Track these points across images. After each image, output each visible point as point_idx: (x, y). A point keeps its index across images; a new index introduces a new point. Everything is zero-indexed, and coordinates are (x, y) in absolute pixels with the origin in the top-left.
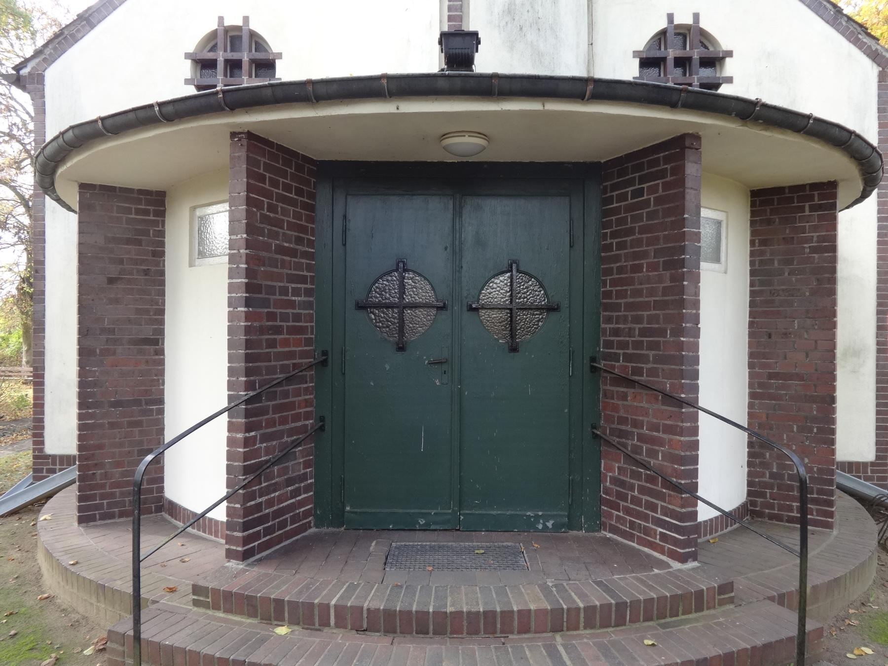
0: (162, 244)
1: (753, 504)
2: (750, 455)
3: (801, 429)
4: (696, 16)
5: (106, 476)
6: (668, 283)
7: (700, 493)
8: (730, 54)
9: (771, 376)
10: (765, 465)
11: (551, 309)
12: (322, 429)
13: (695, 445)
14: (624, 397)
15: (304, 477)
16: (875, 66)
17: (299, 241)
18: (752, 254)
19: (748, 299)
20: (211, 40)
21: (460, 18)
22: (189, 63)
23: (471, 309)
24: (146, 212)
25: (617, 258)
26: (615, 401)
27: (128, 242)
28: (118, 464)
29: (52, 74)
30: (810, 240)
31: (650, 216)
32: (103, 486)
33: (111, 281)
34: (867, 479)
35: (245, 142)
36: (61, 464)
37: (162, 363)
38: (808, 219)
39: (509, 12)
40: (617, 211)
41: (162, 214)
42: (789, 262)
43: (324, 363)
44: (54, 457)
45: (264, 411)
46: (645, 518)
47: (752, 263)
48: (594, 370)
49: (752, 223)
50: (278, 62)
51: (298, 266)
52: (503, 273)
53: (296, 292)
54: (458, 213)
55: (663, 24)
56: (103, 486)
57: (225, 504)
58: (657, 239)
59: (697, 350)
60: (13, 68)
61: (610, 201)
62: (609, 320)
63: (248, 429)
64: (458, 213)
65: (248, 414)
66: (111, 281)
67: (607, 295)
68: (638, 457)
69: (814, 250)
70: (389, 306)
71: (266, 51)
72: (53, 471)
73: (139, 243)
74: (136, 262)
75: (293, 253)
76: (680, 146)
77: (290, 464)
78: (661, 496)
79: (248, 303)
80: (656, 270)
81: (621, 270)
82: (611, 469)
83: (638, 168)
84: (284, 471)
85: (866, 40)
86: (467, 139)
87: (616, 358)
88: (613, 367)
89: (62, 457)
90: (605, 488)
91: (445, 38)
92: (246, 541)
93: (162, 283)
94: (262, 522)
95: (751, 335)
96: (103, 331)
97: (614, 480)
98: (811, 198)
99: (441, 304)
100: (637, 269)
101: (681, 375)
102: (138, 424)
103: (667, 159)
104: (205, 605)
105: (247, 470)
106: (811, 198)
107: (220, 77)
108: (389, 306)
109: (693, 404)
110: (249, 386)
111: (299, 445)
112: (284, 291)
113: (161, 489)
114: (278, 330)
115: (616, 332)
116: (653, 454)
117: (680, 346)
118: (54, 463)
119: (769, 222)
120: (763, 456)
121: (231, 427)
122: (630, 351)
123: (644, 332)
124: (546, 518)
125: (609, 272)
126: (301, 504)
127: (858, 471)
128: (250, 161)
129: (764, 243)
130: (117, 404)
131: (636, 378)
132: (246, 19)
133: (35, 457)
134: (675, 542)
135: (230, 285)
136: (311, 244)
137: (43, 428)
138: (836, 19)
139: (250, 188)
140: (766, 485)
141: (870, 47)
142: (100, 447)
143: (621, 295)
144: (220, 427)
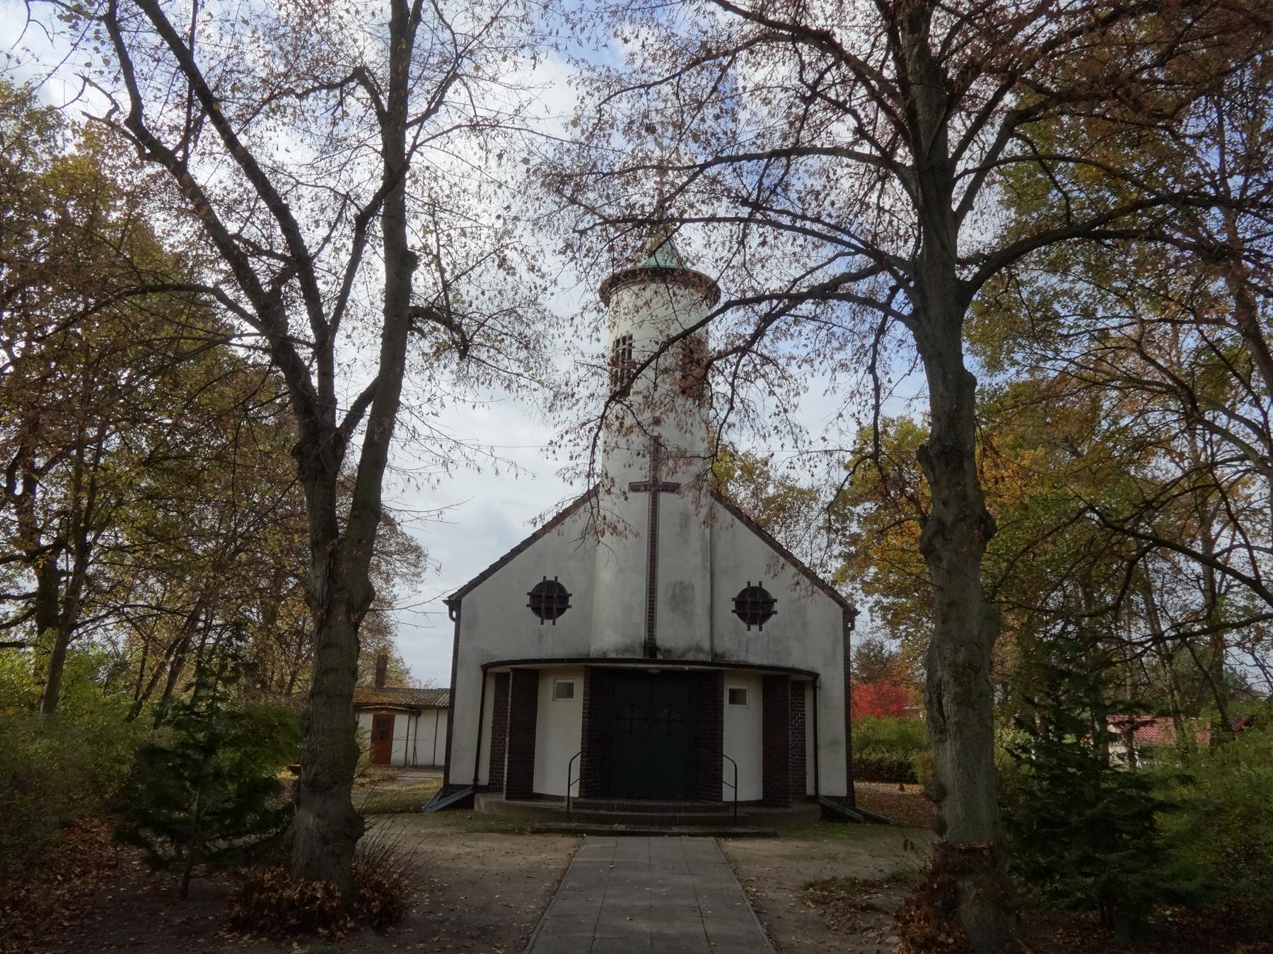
55: (746, 586)
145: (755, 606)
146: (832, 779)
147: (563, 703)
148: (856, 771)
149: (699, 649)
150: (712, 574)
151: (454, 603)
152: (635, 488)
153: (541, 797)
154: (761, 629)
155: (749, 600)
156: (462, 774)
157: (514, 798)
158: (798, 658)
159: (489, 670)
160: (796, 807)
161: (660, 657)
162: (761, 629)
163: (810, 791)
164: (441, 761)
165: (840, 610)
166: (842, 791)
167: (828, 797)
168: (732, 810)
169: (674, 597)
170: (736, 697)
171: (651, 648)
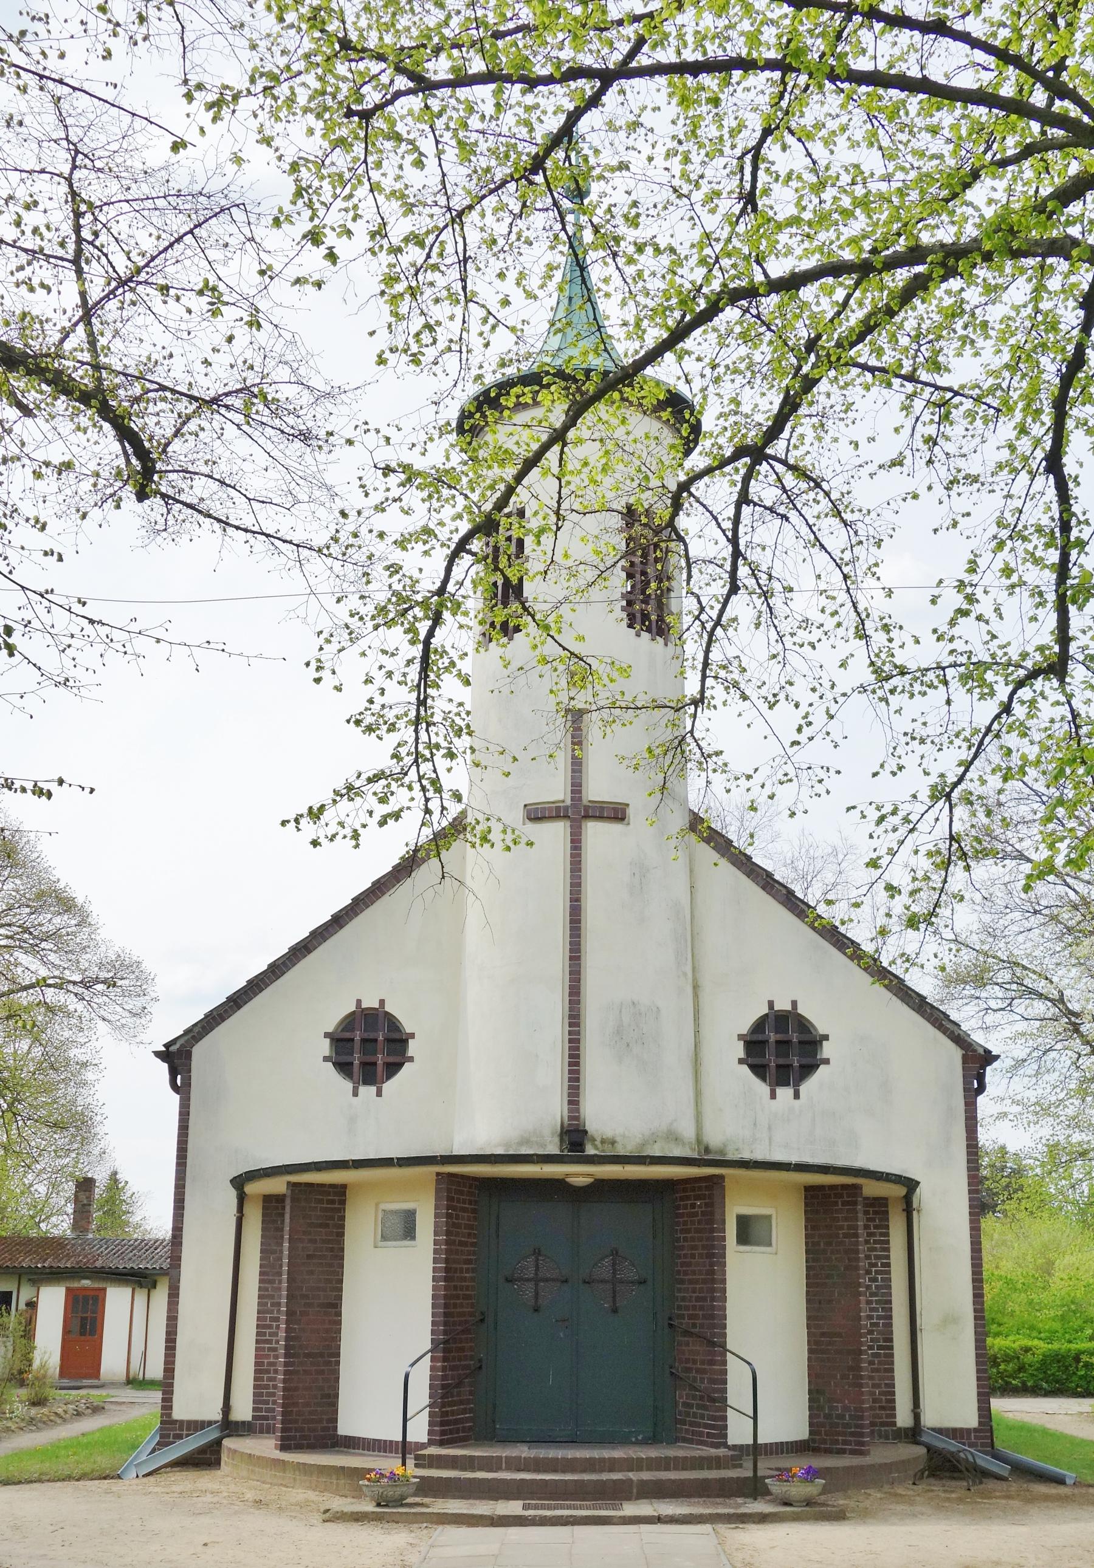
0: (343, 1226)
2: (810, 1400)
3: (843, 1377)
4: (794, 1003)
7: (729, 1402)
8: (826, 1037)
9: (823, 1334)
11: (642, 1282)
13: (725, 1372)
14: (688, 1345)
15: (468, 1402)
22: (328, 1040)
24: (333, 1202)
25: (682, 1248)
27: (321, 1226)
30: (841, 1228)
31: (699, 1222)
32: (296, 1421)
36: (188, 1429)
37: (340, 1323)
40: (682, 1215)
41: (343, 1202)
42: (829, 1244)
43: (482, 1321)
44: (182, 1422)
46: (699, 1425)
48: (671, 1326)
55: (765, 1010)
56: (296, 1421)
61: (678, 1207)
66: (309, 1257)
67: (679, 1272)
69: (846, 1236)
70: (528, 1280)
72: (180, 1437)
73: (327, 1226)
75: (465, 1244)
76: (716, 1182)
81: (685, 1256)
82: (681, 1397)
87: (682, 1317)
89: (189, 1422)
92: (443, 1433)
93: (342, 1258)
94: (449, 1424)
95: (808, 1301)
97: (685, 1404)
98: (841, 1196)
100: (693, 1256)
101: (714, 1326)
102: (322, 1372)
106: (841, 1196)
108: (528, 1280)
109: (723, 1345)
116: (702, 1380)
117: (713, 1308)
121: (433, 1359)
126: (467, 1420)
128: (449, 1190)
129: (813, 1228)
130: (308, 1355)
140: (823, 1425)
142: (296, 1389)
143: (686, 1273)
144: (427, 1361)
145: (783, 1049)
146: (946, 1392)
147: (397, 1253)
148: (998, 1376)
149: (674, 1137)
150: (696, 987)
151: (177, 1057)
152: (537, 814)
153: (352, 1444)
154: (797, 1096)
155: (773, 1037)
156: (198, 1399)
157: (299, 1447)
158: (871, 1148)
159: (251, 1188)
160: (881, 1454)
161: (590, 1150)
162: (797, 1096)
163: (903, 1418)
164: (155, 1370)
165: (956, 1053)
166: (969, 1419)
167: (940, 1431)
168: (748, 1464)
169: (619, 1031)
170: (750, 1231)
171: (574, 1138)
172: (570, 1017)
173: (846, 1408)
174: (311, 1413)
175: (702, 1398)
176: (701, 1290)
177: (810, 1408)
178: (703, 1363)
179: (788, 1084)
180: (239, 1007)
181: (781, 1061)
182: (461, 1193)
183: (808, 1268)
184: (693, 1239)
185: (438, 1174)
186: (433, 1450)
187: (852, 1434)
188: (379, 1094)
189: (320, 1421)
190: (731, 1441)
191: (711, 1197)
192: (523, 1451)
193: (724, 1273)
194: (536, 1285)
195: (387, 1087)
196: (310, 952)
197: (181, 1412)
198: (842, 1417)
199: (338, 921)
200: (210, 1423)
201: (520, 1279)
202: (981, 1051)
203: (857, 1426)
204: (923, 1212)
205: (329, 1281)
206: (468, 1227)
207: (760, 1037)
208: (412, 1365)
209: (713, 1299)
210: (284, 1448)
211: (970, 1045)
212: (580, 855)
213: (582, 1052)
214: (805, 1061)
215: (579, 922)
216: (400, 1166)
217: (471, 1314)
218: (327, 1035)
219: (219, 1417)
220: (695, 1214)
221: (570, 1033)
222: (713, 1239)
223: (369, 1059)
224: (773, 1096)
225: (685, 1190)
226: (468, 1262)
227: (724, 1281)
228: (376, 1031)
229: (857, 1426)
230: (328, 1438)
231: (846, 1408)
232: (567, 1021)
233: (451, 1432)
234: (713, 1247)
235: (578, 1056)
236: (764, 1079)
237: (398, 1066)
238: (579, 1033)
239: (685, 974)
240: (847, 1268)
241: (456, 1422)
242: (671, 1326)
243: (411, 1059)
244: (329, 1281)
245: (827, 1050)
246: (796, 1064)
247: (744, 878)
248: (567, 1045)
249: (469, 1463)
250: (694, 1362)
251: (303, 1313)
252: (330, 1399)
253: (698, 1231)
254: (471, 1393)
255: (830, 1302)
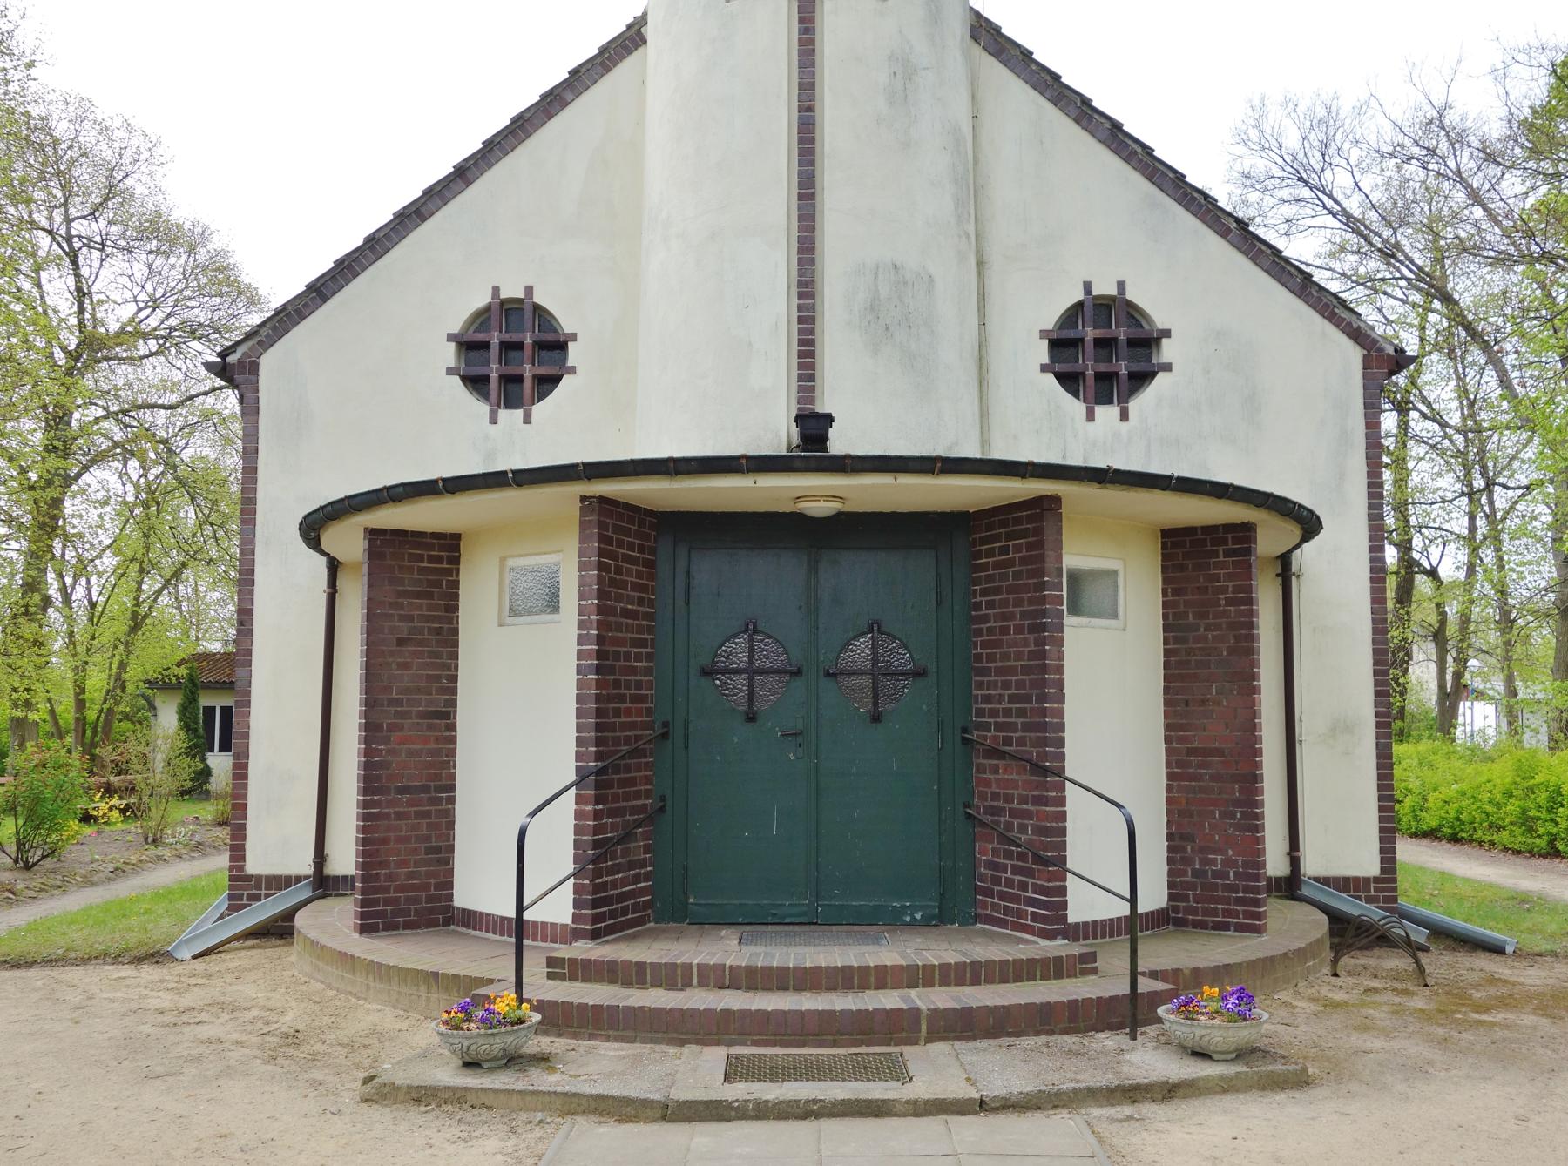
0: (456, 597)
1: (1176, 909)
2: (1170, 849)
3: (1224, 815)
4: (1121, 285)
5: (390, 877)
6: (1032, 648)
7: (1069, 866)
8: (1167, 333)
9: (1191, 752)
10: (1186, 861)
11: (919, 673)
12: (662, 809)
14: (995, 770)
15: (643, 864)
16: (1358, 348)
17: (641, 601)
18: (1165, 605)
19: (1162, 660)
20: (482, 318)
21: (813, 401)
22: (453, 345)
23: (827, 674)
24: (439, 560)
25: (986, 619)
26: (987, 776)
27: (419, 595)
28: (403, 864)
29: (269, 363)
30: (1224, 590)
31: (1017, 575)
32: (387, 890)
33: (401, 642)
34: (1369, 900)
35: (596, 506)
37: (453, 740)
38: (1223, 566)
39: (872, 309)
40: (985, 567)
42: (1202, 616)
43: (665, 736)
44: (259, 878)
45: (609, 785)
46: (1016, 899)
47: (1165, 617)
48: (966, 741)
49: (1164, 569)
50: (570, 344)
51: (640, 629)
52: (863, 634)
53: (638, 658)
54: (813, 569)
55: (1079, 296)
56: (387, 890)
57: (572, 880)
58: (1022, 600)
59: (1062, 717)
60: (219, 355)
61: (978, 555)
62: (980, 686)
63: (598, 800)
64: (813, 569)
65: (598, 785)
66: (401, 642)
67: (978, 658)
68: (1009, 834)
69: (1230, 602)
70: (737, 672)
71: (555, 331)
72: (257, 898)
73: (430, 595)
74: (428, 619)
76: (1046, 507)
77: (632, 845)
78: (1029, 873)
79: (599, 670)
80: (1021, 632)
81: (991, 631)
83: (1004, 524)
84: (626, 852)
85: (1345, 315)
86: (822, 504)
87: (986, 727)
88: (985, 738)
89: (269, 879)
90: (981, 874)
91: (799, 419)
92: (596, 919)
93: (456, 644)
94: (610, 902)
95: (1168, 703)
96: (392, 702)
97: (991, 865)
99: (795, 669)
101: (1044, 742)
102: (427, 815)
103: (1030, 519)
104: (562, 977)
105: (596, 844)
106: (1224, 541)
107: (494, 366)
108: (737, 672)
109: (1060, 772)
110: (599, 756)
111: (639, 826)
112: (627, 657)
113: (450, 897)
114: (622, 698)
115: (988, 699)
116: (1023, 829)
117: (1043, 713)
118: (258, 887)
119: (1182, 568)
120: (1184, 850)
121: (579, 800)
122: (1001, 720)
123: (1012, 699)
124: (914, 909)
125: (979, 633)
126: (642, 892)
127: (1357, 890)
128: (602, 526)
129: (1176, 592)
130: (404, 790)
131: (1007, 748)
132: (529, 290)
133: (232, 879)
134: (1045, 919)
135: (579, 652)
136: (651, 604)
137: (244, 837)
138: (1304, 287)
139: (601, 553)
141: (1350, 324)
142: (385, 841)
143: (991, 658)
144: (569, 800)
145: (1105, 350)
150: (980, 264)
154: (1124, 416)
162: (1124, 416)
163: (1275, 864)
165: (1355, 354)
166: (1370, 866)
167: (1326, 881)
169: (873, 306)
172: (800, 284)
173: (1228, 863)
174: (411, 876)
175: (1022, 857)
176: (1020, 684)
177: (1170, 861)
178: (1023, 800)
179: (1110, 402)
180: (325, 299)
181: (1103, 368)
182: (627, 532)
183: (1167, 653)
184: (1005, 603)
185: (583, 499)
186: (583, 950)
187: (1239, 901)
188: (527, 419)
189: (426, 887)
190: (1071, 920)
191: (1039, 532)
192: (725, 949)
193: (1061, 657)
194: (751, 680)
195: (538, 409)
196: (424, 219)
197: (256, 864)
198: (1223, 875)
199: (464, 174)
200: (298, 879)
201: (726, 671)
202: (1391, 351)
203: (1246, 889)
204: (1302, 579)
205: (437, 678)
206: (636, 587)
207: (1071, 334)
208: (533, 814)
209: (1043, 698)
210: (367, 926)
211: (1375, 342)
212: (812, 41)
213: (818, 337)
214: (1136, 367)
215: (813, 141)
216: (519, 485)
217: (647, 726)
218: (451, 337)
219: (308, 869)
220: (1011, 563)
221: (800, 308)
222: (1043, 600)
223: (512, 370)
224: (1090, 417)
225: (990, 527)
226: (642, 643)
227: (1060, 669)
228: (520, 329)
229: (1246, 889)
230: (434, 911)
231: (1228, 863)
232: (794, 291)
233: (613, 914)
234: (1044, 613)
235: (812, 343)
236: (1076, 394)
237: (555, 380)
238: (813, 308)
239: (968, 236)
240: (1232, 651)
241: (622, 897)
242: (966, 741)
243: (572, 370)
244: (437, 678)
245: (1168, 351)
246: (1124, 371)
247: (1048, 106)
248: (795, 327)
249: (637, 975)
250: (1009, 799)
251: (392, 728)
252: (442, 855)
253: (1010, 590)
254: (647, 849)
255: (1204, 702)
